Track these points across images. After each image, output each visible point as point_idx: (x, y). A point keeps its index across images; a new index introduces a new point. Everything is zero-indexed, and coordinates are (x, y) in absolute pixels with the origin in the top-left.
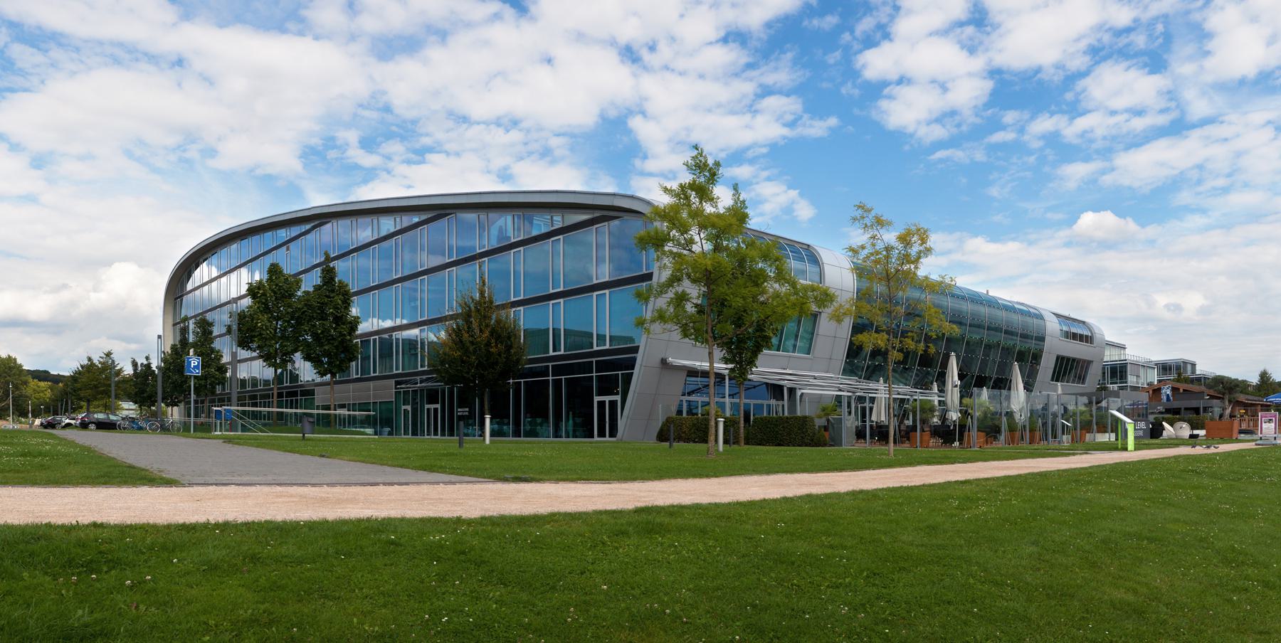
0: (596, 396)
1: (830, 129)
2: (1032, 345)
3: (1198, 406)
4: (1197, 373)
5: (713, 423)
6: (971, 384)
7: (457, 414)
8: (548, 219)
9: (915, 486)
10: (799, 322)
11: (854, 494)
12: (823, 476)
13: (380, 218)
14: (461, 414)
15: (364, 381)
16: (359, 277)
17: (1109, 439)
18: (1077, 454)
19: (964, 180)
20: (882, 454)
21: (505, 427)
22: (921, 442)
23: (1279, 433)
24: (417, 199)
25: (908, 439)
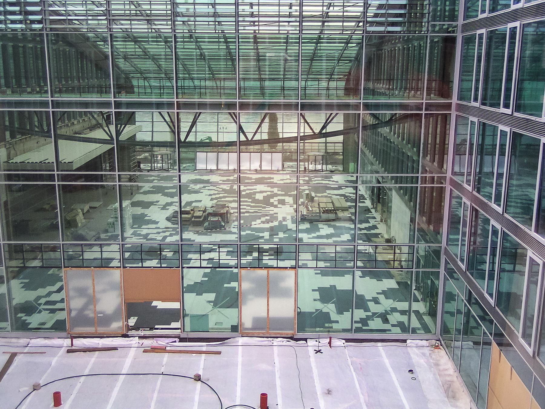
0: (5, 294)
1: (482, 241)
2: (536, 143)
3: (4, 187)
4: (486, 156)
5: (534, 117)
6: (378, 16)
7: (61, 250)
8: (243, 209)
9: (7, 230)
10: (94, 291)
11: (478, 98)
12: (445, 223)
13: (265, 315)
14: (174, 325)
15: (194, 351)
16: (504, 238)
17: (261, 166)
18: (210, 175)
19: (525, 161)
20: (212, 88)
21: (397, 37)
22: (63, 238)
23: (2, 296)
24: (67, 380)
25: (229, 106)
